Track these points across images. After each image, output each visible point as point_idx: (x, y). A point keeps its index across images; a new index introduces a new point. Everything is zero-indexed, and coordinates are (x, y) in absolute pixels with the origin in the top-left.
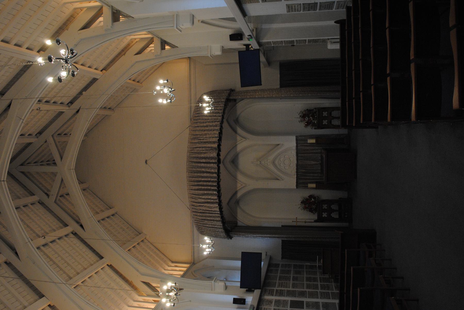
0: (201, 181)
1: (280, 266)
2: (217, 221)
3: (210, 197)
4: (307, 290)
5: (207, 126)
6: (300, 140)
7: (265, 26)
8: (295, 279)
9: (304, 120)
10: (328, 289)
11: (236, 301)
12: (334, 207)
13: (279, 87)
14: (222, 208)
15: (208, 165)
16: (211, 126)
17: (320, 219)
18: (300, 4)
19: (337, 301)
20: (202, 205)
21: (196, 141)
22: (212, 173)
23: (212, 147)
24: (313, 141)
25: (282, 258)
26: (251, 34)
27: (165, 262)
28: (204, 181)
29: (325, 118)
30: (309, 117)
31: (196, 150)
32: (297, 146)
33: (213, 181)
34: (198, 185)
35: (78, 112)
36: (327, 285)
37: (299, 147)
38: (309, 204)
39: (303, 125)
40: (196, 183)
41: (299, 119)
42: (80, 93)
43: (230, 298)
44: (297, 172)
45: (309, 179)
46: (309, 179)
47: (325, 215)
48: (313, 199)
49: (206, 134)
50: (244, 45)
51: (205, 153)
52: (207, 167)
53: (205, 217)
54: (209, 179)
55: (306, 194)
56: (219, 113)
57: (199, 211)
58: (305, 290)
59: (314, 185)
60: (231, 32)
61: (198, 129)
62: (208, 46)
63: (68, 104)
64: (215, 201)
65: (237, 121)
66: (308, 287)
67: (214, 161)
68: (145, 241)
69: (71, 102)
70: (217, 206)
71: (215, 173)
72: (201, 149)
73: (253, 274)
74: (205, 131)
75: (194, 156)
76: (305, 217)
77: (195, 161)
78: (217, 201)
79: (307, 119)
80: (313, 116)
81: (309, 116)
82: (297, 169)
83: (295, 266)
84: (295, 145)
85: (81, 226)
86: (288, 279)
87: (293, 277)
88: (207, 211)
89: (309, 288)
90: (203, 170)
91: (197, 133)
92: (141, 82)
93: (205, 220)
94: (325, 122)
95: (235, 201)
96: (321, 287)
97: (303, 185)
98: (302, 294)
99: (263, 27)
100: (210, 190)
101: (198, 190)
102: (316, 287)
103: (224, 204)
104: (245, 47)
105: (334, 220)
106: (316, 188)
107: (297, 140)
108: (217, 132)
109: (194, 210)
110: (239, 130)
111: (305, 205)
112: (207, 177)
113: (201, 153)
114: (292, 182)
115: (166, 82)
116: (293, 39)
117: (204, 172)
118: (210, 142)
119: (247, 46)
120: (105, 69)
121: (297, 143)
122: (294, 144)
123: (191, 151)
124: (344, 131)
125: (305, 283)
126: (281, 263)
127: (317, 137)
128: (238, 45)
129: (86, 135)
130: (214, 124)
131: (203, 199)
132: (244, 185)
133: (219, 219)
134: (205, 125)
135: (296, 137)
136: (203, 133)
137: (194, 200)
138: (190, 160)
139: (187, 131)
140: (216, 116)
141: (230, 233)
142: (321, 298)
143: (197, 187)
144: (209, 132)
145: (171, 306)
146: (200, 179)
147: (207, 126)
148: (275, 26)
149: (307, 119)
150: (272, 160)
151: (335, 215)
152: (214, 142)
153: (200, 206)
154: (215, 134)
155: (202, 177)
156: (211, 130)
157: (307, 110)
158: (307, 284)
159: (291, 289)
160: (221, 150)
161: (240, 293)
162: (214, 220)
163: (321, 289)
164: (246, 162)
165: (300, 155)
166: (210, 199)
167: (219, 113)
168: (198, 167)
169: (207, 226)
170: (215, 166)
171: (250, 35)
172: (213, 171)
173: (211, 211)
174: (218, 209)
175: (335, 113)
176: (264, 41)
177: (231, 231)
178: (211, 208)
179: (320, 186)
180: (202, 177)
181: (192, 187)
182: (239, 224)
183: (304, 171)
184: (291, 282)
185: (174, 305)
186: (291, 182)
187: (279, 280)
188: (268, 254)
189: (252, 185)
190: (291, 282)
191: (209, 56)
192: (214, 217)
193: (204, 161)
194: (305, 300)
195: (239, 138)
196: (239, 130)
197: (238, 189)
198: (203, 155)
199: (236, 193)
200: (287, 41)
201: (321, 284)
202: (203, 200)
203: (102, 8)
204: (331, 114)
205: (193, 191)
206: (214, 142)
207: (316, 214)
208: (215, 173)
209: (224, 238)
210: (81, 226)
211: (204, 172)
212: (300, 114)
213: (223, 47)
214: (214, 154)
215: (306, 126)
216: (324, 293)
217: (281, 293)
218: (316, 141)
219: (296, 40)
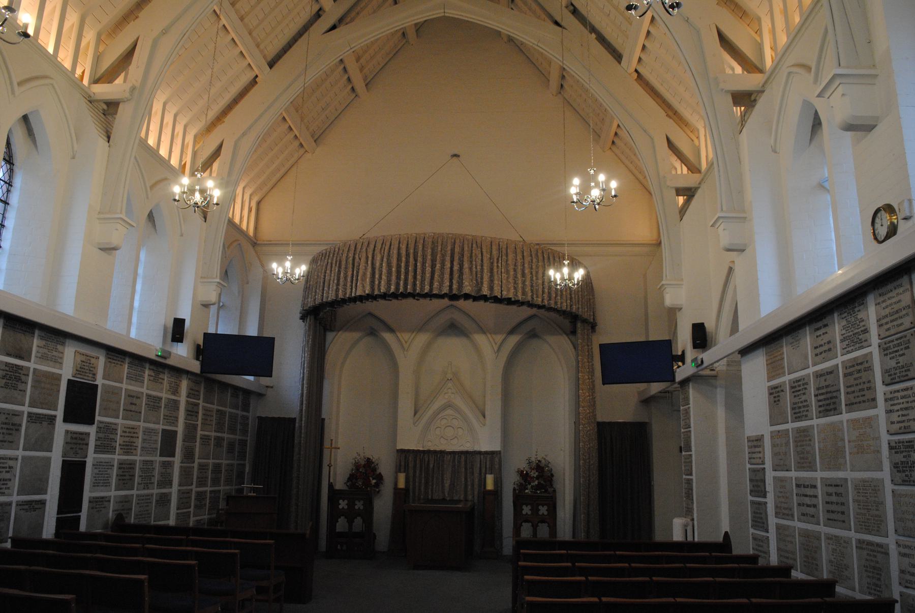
0: (416, 260)
1: (245, 413)
2: (337, 290)
3: (384, 277)
4: (196, 465)
5: (523, 275)
7: (720, 394)
10: (196, 506)
11: (179, 324)
13: (599, 419)
14: (361, 302)
15: (447, 276)
16: (524, 282)
17: (334, 495)
18: (763, 464)
19: (172, 522)
20: (369, 262)
21: (495, 252)
23: (482, 283)
24: (490, 486)
26: (705, 365)
28: (416, 265)
29: (535, 511)
30: (537, 478)
31: (476, 252)
32: (480, 453)
33: (414, 284)
34: (408, 255)
35: (557, 23)
36: (205, 504)
37: (478, 457)
38: (365, 474)
39: (523, 466)
40: (412, 251)
41: (533, 459)
42: (593, 29)
43: (185, 313)
44: (429, 452)
45: (414, 476)
46: (414, 476)
47: (343, 504)
48: (374, 481)
49: (507, 272)
50: (683, 352)
51: (471, 269)
52: (442, 274)
54: (419, 277)
55: (386, 468)
56: (550, 299)
57: (357, 256)
58: (197, 461)
59: (402, 484)
60: (710, 326)
61: (519, 257)
62: (682, 280)
63: (572, 4)
64: (376, 287)
65: (533, 335)
66: (202, 467)
67: (455, 286)
68: (302, 151)
69: (575, 12)
70: (367, 292)
71: (431, 290)
74: (515, 270)
75: (466, 248)
76: (339, 467)
77: (454, 251)
78: (376, 292)
79: (534, 474)
80: (539, 486)
82: (435, 452)
83: (243, 443)
85: (334, 27)
86: (220, 428)
88: (358, 272)
89: (199, 469)
90: (438, 266)
91: (511, 256)
92: (614, 148)
93: (340, 267)
94: (526, 510)
95: (374, 328)
96: (201, 492)
97: (403, 463)
98: (189, 455)
99: (718, 390)
100: (398, 278)
101: (399, 255)
102: (202, 482)
103: (370, 306)
104: (680, 353)
106: (396, 488)
107: (492, 453)
108: (511, 296)
109: (359, 247)
110: (514, 339)
111: (364, 466)
112: (423, 272)
114: (409, 441)
115: (613, 193)
116: (693, 449)
117: (433, 266)
118: (491, 281)
119: (682, 358)
120: (639, 76)
121: (486, 453)
122: (484, 448)
123: (475, 243)
126: (250, 415)
127: (497, 493)
128: (684, 340)
129: (511, 40)
131: (381, 264)
132: (406, 346)
133: (341, 295)
135: (499, 453)
136: (511, 268)
137: (379, 246)
138: (457, 241)
139: (514, 237)
141: (312, 317)
142: (179, 491)
143: (403, 252)
144: (511, 280)
145: (174, 194)
146: (420, 259)
147: (523, 275)
148: (721, 413)
149: (534, 474)
150: (456, 403)
151: (341, 525)
152: (491, 288)
153: (367, 258)
154: (508, 290)
155: (424, 264)
157: (552, 475)
158: (207, 465)
159: (199, 433)
161: (194, 333)
162: (338, 284)
164: (452, 352)
165: (463, 457)
167: (550, 299)
168: (443, 256)
170: (445, 290)
171: (702, 362)
172: (436, 284)
173: (357, 280)
174: (359, 292)
176: (692, 392)
177: (315, 319)
178: (362, 280)
179: (400, 495)
180: (424, 264)
181: (405, 242)
182: (330, 336)
183: (431, 466)
185: (175, 200)
186: (410, 439)
188: (269, 389)
189: (406, 361)
191: (664, 282)
192: (345, 285)
193: (456, 268)
194: (177, 460)
195: (499, 338)
196: (514, 339)
197: (399, 335)
198: (466, 265)
199: (391, 330)
200: (690, 437)
201: (206, 492)
202: (378, 264)
203: (761, 71)
204: (543, 522)
206: (491, 288)
207: (345, 488)
208: (431, 290)
209: (303, 305)
210: (334, 27)
211: (433, 266)
212: (543, 461)
213: (680, 309)
214: (468, 289)
215: (521, 473)
217: (192, 412)
218: (490, 491)
219: (691, 455)
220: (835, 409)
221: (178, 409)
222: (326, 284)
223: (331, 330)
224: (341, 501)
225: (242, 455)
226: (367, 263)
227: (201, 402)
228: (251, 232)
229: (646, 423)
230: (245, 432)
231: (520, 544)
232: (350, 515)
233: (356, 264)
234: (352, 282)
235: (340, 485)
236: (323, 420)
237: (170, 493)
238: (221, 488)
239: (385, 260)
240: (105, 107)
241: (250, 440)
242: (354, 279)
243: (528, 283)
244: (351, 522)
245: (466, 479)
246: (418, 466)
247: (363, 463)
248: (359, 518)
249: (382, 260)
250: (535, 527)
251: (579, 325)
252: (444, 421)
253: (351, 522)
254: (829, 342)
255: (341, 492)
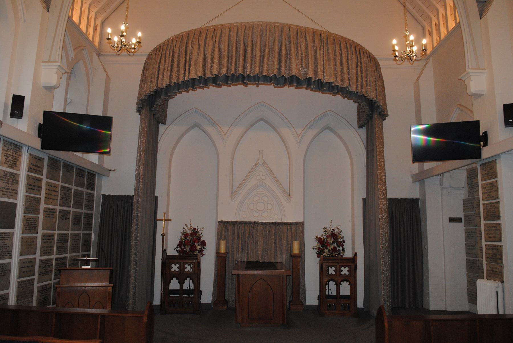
1: (90, 191)
2: (171, 76)
3: (216, 61)
4: (39, 236)
5: (341, 64)
6: (296, 229)
8: (64, 215)
9: (328, 236)
10: (40, 273)
11: (18, 102)
12: (188, 284)
13: (389, 196)
17: (167, 261)
21: (317, 42)
22: (261, 66)
24: (296, 251)
25: (104, 196)
27: (103, 9)
29: (338, 271)
30: (333, 242)
32: (287, 223)
36: (51, 271)
39: (320, 234)
41: (328, 229)
43: (26, 92)
44: (245, 223)
47: (175, 268)
49: (329, 60)
50: (485, 133)
53: (179, 56)
55: (209, 236)
56: (362, 88)
58: (40, 231)
66: (47, 238)
67: (283, 69)
70: (200, 75)
72: (303, 48)
73: (70, 133)
74: (335, 59)
78: (209, 75)
81: (330, 246)
83: (89, 217)
84: (289, 221)
86: (65, 202)
87: (68, 212)
88: (190, 59)
89: (43, 239)
93: (173, 56)
96: (46, 260)
98: (30, 226)
102: (46, 251)
105: (166, 282)
106: (218, 253)
107: (297, 224)
110: (312, 133)
111: (191, 234)
113: (297, 49)
118: (316, 66)
119: (485, 138)
121: (292, 224)
122: (290, 219)
124: (312, 298)
125: (56, 232)
130: (346, 76)
133: (174, 80)
134: (344, 61)
140: (357, 82)
147: (341, 64)
151: (174, 285)
152: (316, 73)
156: (335, 69)
157: (344, 241)
158: (53, 235)
159: (43, 206)
160: (298, 90)
162: (171, 71)
163: (42, 261)
165: (273, 229)
166: (212, 62)
167: (362, 88)
169: (163, 62)
174: (193, 75)
175: (345, 289)
177: (151, 111)
183: (247, 235)
184: (58, 208)
187: (63, 187)
190: (58, 208)
192: (178, 71)
196: (312, 133)
199: (213, 123)
201: (52, 259)
202: (210, 49)
205: (227, 33)
206: (316, 73)
207: (175, 253)
209: (139, 94)
212: (336, 230)
213: (478, 96)
215: (320, 240)
216: (33, 266)
217: (33, 185)
220: (44, 236)
221: (17, 182)
222: (161, 72)
223: (164, 123)
224: (173, 265)
225: (88, 226)
226: (199, 49)
227: (44, 177)
228: (97, 43)
229: (417, 200)
230: (90, 207)
231: (323, 296)
232: (181, 277)
233: (188, 52)
234: (185, 68)
235: (172, 251)
236: (157, 197)
237: (10, 264)
238: (68, 255)
239: (217, 45)
240: (261, 162)
241: (96, 213)
242: (188, 65)
243: (345, 71)
244: (181, 283)
245: (276, 244)
246: (236, 235)
247: (189, 232)
248: (175, 279)
249: (214, 46)
250: (338, 285)
251: (376, 116)
252: (256, 198)
253: (181, 283)
254: (50, 247)
255: (172, 257)
